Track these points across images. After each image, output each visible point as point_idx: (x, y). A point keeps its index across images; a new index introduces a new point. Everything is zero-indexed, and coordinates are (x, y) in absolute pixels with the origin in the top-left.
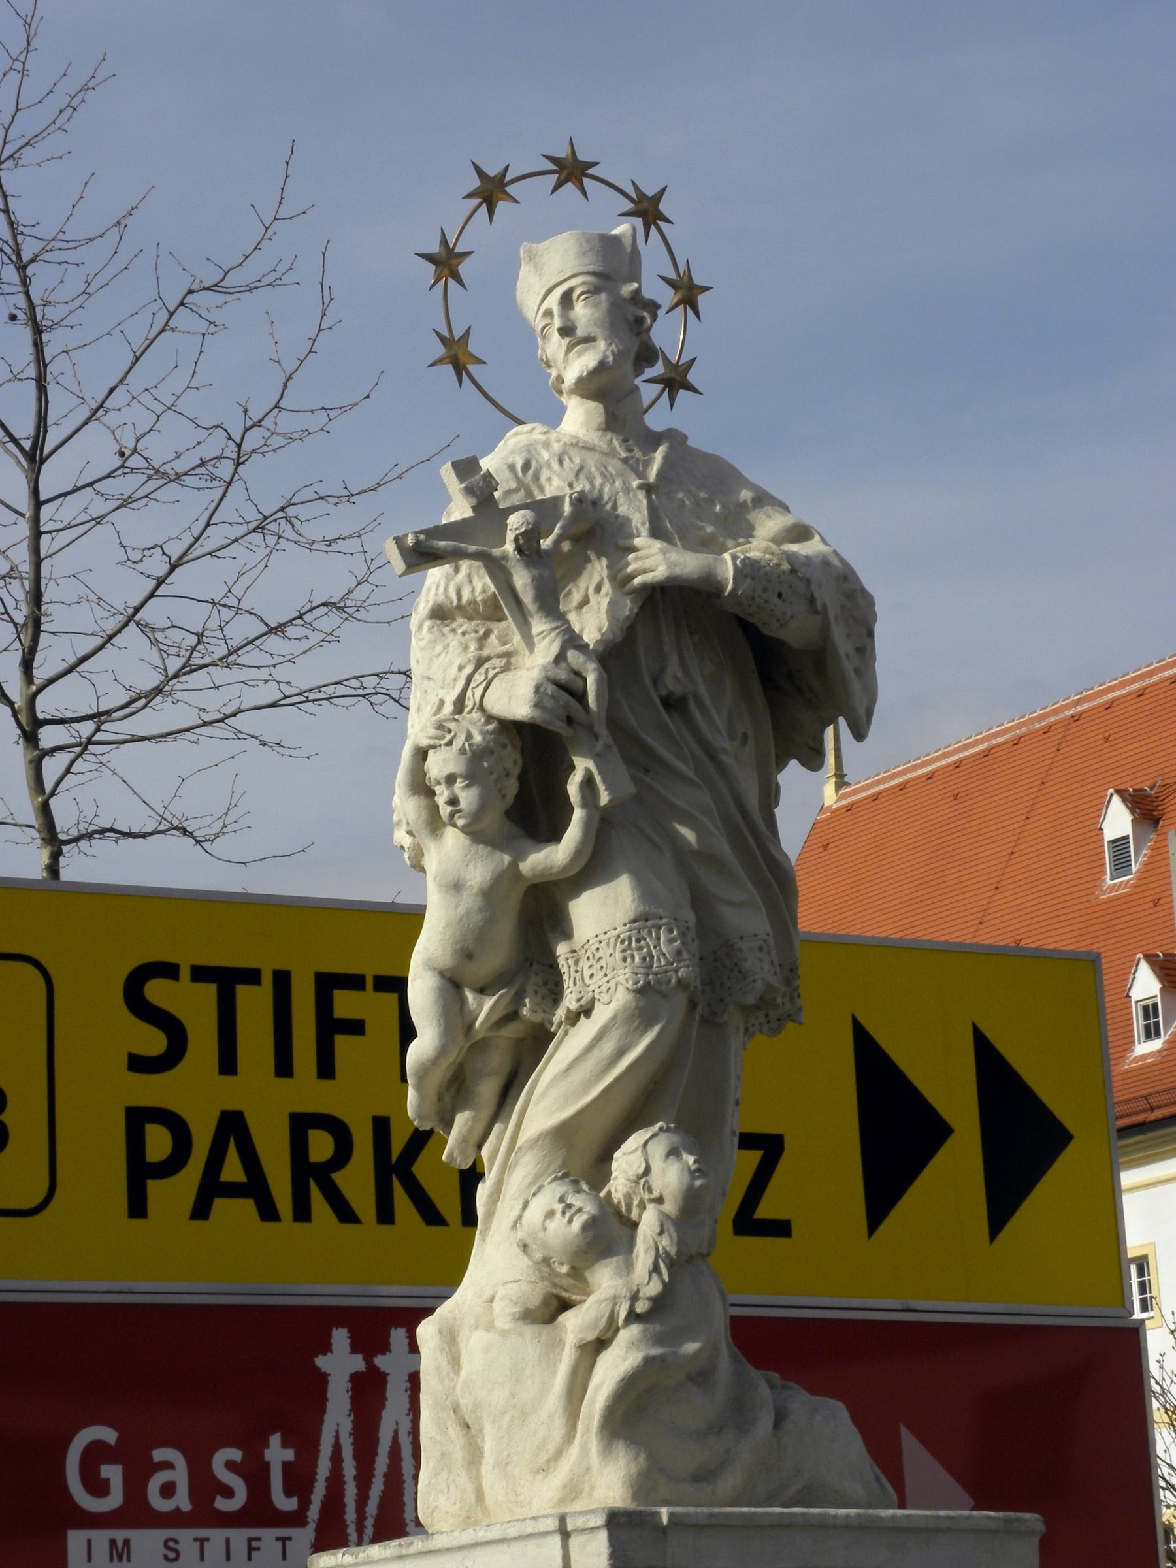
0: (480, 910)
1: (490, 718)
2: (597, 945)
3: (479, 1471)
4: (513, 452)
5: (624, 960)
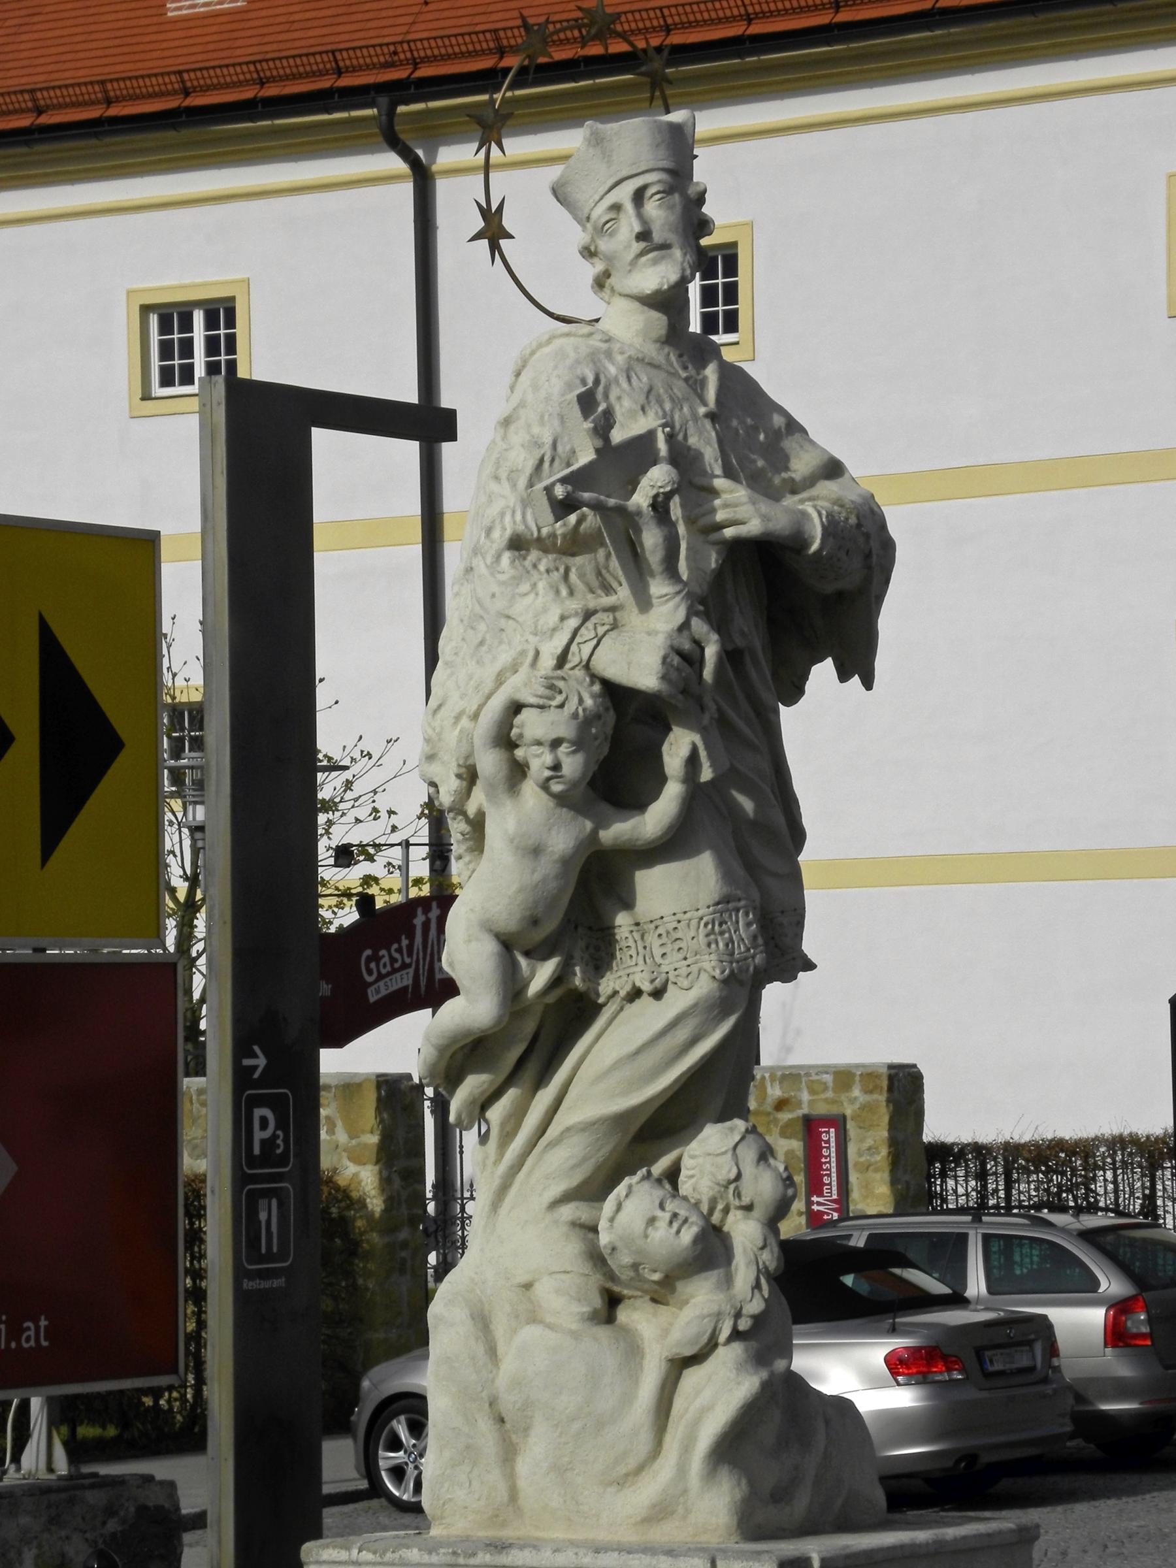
0: (557, 877)
1: (594, 677)
2: (675, 924)
3: (513, 1469)
4: (578, 362)
5: (709, 945)
